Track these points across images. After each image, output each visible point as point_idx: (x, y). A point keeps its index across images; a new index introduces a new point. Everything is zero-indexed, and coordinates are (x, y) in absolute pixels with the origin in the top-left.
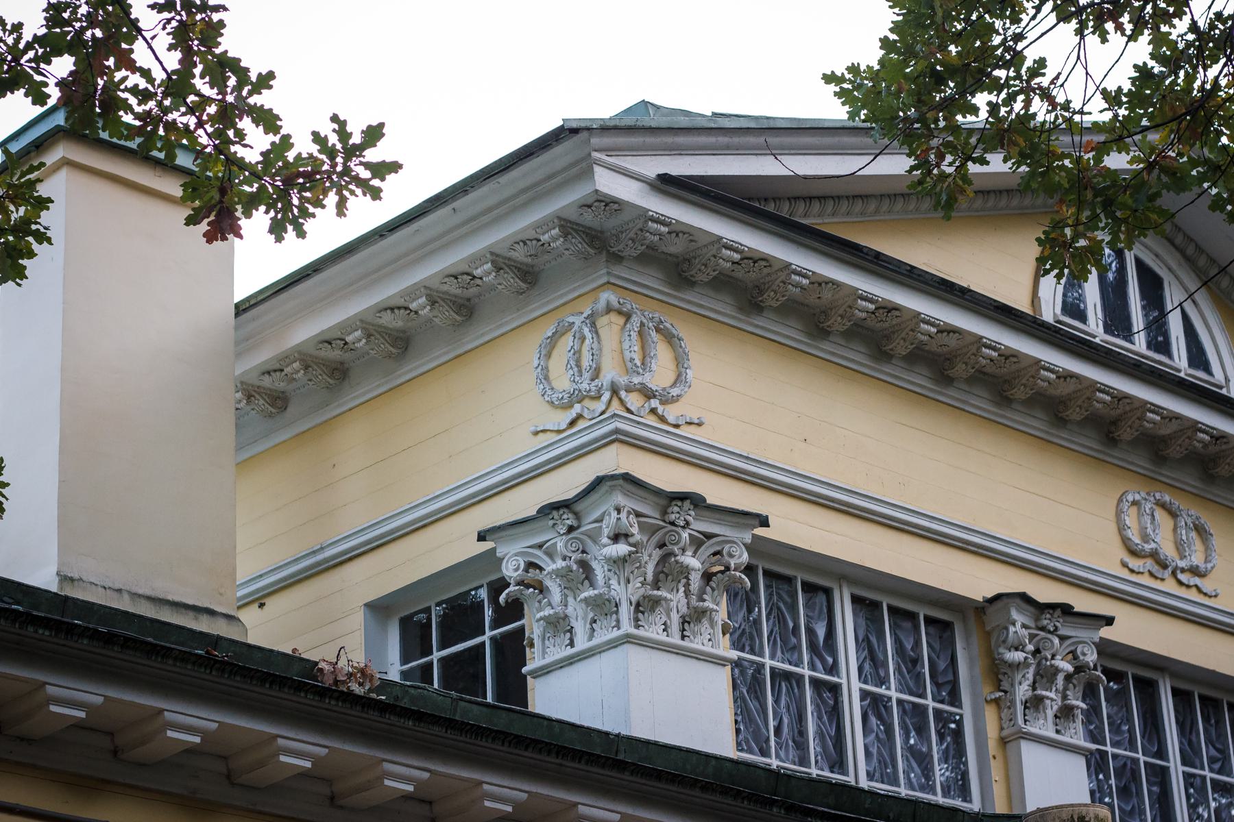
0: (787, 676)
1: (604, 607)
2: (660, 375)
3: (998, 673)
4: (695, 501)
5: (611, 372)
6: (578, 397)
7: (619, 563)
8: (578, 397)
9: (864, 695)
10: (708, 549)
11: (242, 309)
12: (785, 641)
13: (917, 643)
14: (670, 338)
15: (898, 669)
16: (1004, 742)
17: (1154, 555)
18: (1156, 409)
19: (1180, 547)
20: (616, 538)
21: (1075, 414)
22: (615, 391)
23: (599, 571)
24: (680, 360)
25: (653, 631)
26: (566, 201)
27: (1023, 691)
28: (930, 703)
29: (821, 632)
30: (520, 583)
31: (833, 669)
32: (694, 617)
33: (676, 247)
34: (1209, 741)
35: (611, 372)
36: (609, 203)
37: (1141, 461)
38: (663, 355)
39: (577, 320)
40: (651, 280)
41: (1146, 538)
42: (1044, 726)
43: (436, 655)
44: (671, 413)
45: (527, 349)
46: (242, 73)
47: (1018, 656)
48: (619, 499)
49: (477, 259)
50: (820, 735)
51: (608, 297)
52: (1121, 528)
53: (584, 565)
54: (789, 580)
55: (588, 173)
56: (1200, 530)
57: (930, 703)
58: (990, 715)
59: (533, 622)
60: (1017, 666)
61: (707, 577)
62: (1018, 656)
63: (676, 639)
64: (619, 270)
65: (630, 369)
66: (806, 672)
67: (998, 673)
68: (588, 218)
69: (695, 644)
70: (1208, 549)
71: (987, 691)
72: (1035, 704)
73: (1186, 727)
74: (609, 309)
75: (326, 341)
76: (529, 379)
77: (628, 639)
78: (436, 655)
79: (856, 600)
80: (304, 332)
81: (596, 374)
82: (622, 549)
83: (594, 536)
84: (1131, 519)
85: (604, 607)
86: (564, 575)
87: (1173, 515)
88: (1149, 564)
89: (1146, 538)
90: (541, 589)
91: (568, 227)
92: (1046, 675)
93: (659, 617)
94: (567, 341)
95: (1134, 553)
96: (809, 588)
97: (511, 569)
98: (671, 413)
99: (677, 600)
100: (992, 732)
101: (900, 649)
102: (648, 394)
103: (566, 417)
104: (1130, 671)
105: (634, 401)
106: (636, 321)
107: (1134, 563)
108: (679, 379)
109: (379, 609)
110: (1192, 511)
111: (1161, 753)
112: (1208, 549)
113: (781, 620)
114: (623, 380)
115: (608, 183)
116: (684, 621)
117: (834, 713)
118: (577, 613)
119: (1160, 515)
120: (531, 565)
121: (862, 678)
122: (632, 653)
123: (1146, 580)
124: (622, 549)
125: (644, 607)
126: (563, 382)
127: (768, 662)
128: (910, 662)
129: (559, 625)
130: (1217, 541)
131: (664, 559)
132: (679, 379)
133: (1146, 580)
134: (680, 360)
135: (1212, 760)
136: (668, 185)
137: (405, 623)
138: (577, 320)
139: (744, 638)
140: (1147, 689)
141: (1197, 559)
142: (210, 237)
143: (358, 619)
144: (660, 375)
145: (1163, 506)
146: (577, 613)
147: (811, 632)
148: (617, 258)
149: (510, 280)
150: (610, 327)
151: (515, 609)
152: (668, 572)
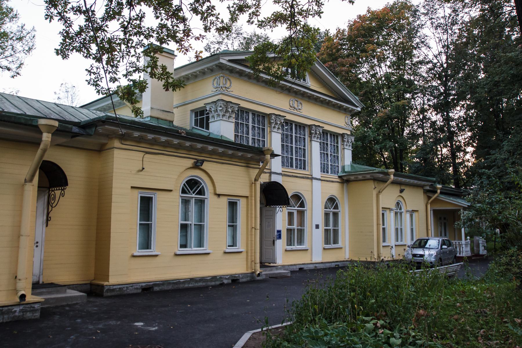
0: (242, 123)
1: (219, 115)
2: (228, 85)
3: (270, 123)
4: (231, 102)
5: (221, 85)
6: (217, 88)
7: (221, 110)
8: (217, 88)
9: (252, 126)
10: (232, 108)
11: (175, 70)
12: (242, 119)
13: (260, 119)
14: (230, 80)
15: (257, 122)
16: (270, 132)
17: (294, 107)
18: (295, 88)
19: (298, 106)
20: (220, 107)
21: (284, 89)
22: (221, 87)
23: (218, 111)
24: (231, 83)
25: (224, 119)
26: (216, 62)
27: (273, 125)
28: (261, 127)
29: (247, 118)
30: (209, 111)
31: (248, 122)
32: (230, 117)
33: (231, 68)
34: (299, 131)
35: (221, 85)
36: (222, 63)
37: (294, 95)
38: (228, 82)
39: (218, 77)
40: (227, 72)
41: (293, 105)
42: (276, 130)
43: (199, 118)
44: (229, 90)
45: (211, 80)
46: (169, 73)
47: (273, 121)
48: (221, 102)
49: (205, 68)
50: (246, 131)
51: (221, 75)
52: (290, 104)
53: (217, 109)
54: (244, 111)
55: (219, 59)
56: (301, 103)
57: (261, 127)
58: (269, 128)
59: (210, 115)
60: (272, 122)
61: (232, 111)
62: (273, 121)
63: (227, 120)
64: (223, 71)
65: (224, 84)
66: (245, 123)
67: (270, 123)
68: (219, 65)
69: (230, 120)
70: (302, 106)
71: (269, 125)
72: (274, 127)
73: (296, 129)
74: (221, 76)
75: (186, 75)
76: (211, 84)
77: (221, 120)
78: (199, 118)
79: (252, 113)
80: (183, 74)
81: (219, 85)
82: (221, 108)
83: (218, 106)
84: (291, 103)
85: (219, 115)
86: (214, 111)
87: (297, 101)
88: (293, 108)
89: (293, 105)
90: (211, 112)
91: (216, 65)
92: (276, 124)
93: (225, 117)
94: (216, 80)
95: (291, 107)
96: (246, 112)
97: (208, 109)
98: (229, 90)
99: (228, 115)
100: (269, 131)
101: (258, 119)
102: (226, 88)
103: (215, 90)
104: (289, 122)
105: (224, 89)
106: (225, 78)
107: (291, 108)
108: (230, 86)
109: (192, 111)
110: (300, 101)
111: (292, 133)
112: (302, 106)
113: (242, 116)
114: (223, 86)
115: (222, 61)
116: (229, 117)
117: (248, 128)
118: (215, 115)
119: (295, 102)
120: (210, 109)
121: (252, 123)
122: (222, 122)
123: (292, 111)
124: (221, 108)
125: (223, 116)
126: (215, 85)
127: (240, 122)
128: (259, 121)
129: (213, 117)
130: (303, 105)
131: (226, 109)
132: (230, 86)
133: (292, 111)
134: (231, 83)
135: (299, 133)
136: (230, 61)
137: (195, 113)
138: (218, 77)
139: (237, 118)
140: (291, 124)
141: (300, 108)
142: (166, 91)
143: (189, 112)
144: (228, 85)
145: (296, 100)
146: (215, 115)
147: (246, 118)
148: (223, 70)
149: (209, 71)
150: (222, 79)
151: (208, 114)
152: (227, 111)
